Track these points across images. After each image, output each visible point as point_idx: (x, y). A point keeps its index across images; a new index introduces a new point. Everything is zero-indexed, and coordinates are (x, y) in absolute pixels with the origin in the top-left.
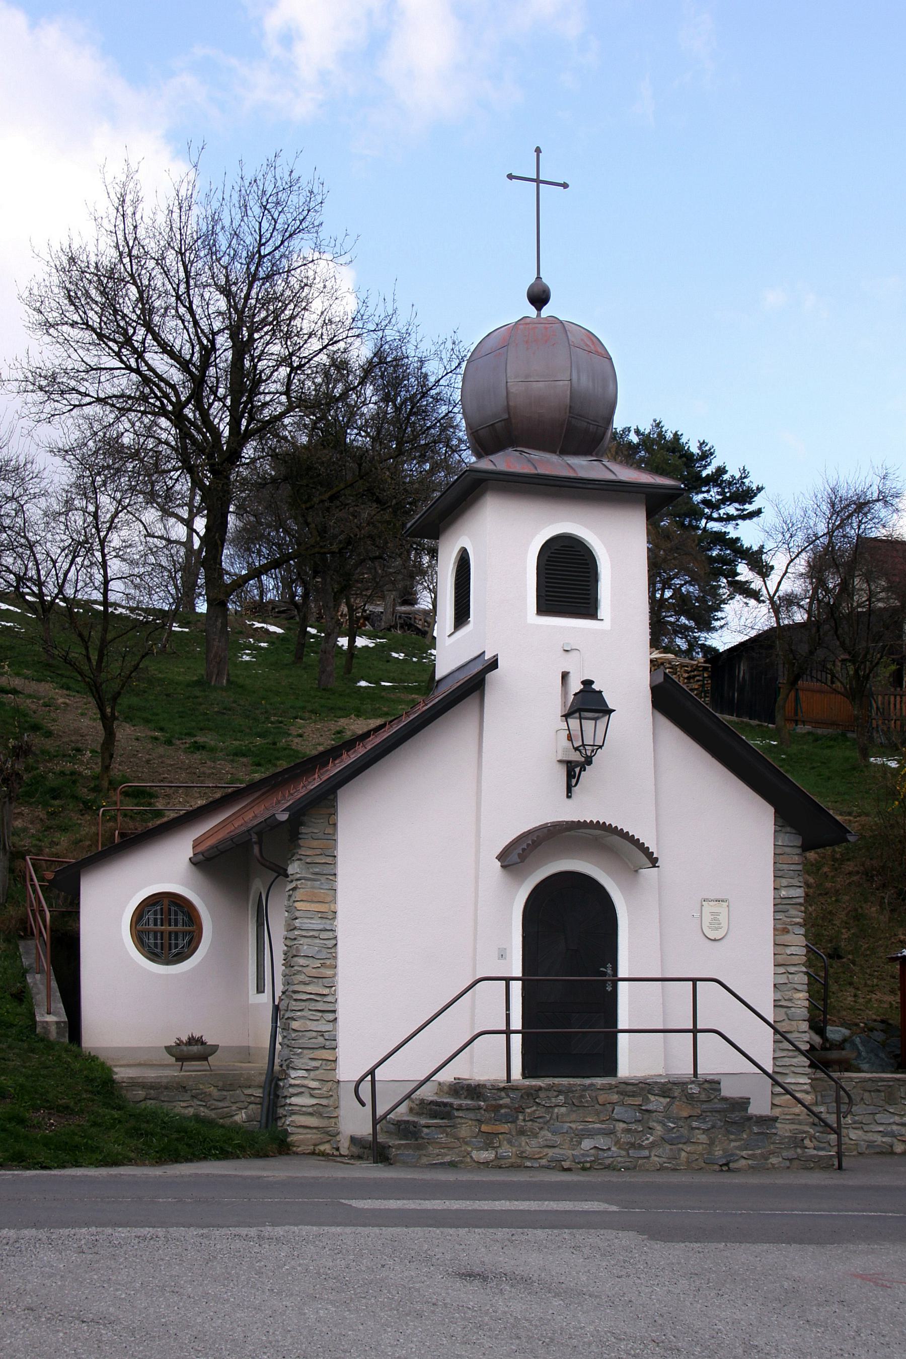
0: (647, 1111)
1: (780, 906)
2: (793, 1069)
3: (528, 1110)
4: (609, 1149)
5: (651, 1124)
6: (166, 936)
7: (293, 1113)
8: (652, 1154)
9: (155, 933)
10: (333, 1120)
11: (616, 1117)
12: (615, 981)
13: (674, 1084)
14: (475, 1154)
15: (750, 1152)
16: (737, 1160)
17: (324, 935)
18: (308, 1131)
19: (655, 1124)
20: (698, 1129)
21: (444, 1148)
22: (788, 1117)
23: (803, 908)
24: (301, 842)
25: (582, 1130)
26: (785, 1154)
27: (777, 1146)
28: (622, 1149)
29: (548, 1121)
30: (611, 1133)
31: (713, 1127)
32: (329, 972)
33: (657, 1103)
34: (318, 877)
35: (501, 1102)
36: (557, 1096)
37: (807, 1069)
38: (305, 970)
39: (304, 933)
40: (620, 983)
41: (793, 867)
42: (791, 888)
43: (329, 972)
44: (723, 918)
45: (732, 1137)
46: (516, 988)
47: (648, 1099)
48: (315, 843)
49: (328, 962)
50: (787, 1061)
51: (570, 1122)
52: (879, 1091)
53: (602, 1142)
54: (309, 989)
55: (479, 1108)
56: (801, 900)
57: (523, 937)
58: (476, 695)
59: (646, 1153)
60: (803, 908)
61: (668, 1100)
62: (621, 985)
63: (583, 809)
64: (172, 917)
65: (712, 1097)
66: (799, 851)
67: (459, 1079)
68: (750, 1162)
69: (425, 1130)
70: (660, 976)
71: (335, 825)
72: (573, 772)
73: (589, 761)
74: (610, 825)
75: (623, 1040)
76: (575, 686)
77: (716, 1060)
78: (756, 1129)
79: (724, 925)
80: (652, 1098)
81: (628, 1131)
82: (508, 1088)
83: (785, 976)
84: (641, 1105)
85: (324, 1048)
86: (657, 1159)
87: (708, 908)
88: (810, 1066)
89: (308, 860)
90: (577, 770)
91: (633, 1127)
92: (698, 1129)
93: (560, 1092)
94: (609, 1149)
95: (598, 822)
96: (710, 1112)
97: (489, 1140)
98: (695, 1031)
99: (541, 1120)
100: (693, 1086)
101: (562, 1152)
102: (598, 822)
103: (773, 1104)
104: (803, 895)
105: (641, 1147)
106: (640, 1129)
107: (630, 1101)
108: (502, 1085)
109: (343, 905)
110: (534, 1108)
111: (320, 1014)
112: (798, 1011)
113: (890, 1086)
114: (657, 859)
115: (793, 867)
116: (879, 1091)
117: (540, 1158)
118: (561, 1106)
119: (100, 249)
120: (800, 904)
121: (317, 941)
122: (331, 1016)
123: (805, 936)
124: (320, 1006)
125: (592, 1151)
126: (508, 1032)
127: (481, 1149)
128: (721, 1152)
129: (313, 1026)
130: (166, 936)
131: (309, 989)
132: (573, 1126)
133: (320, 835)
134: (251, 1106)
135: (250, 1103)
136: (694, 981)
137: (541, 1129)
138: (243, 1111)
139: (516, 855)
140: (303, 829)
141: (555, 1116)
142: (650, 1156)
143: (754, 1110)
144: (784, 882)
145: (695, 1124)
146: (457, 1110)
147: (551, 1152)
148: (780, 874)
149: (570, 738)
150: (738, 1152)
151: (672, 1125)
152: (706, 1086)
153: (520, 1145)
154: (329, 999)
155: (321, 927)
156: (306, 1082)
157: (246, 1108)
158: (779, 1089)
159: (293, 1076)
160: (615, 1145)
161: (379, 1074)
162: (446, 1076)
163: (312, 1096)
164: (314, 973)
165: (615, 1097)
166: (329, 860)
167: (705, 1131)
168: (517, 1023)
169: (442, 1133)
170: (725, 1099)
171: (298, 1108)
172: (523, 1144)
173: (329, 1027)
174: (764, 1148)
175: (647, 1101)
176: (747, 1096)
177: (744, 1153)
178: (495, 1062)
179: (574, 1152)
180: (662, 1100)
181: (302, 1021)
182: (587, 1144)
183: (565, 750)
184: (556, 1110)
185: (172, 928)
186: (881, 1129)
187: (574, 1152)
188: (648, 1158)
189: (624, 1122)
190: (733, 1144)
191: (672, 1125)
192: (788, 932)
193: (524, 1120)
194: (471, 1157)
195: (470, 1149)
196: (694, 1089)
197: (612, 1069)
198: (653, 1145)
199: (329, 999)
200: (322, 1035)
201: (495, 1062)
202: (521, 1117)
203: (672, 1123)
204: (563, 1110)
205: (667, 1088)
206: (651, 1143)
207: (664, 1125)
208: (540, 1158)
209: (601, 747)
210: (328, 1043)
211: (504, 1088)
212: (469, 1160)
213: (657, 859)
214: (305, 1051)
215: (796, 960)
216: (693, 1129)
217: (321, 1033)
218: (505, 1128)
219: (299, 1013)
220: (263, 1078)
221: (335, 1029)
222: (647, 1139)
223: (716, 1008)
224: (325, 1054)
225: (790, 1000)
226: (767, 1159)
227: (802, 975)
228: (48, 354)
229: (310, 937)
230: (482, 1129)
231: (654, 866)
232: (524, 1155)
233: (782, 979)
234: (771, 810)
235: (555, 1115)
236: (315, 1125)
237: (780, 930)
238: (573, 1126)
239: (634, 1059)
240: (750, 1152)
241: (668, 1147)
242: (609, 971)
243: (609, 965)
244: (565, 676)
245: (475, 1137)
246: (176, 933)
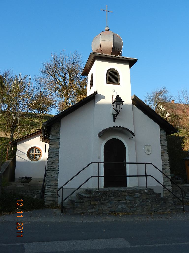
0: (135, 197)
1: (162, 147)
2: (167, 184)
3: (104, 198)
4: (125, 208)
5: (136, 201)
6: (35, 155)
7: (46, 197)
8: (137, 209)
9: (33, 155)
10: (57, 199)
11: (127, 199)
12: (126, 163)
13: (142, 190)
14: (89, 210)
15: (162, 208)
16: (159, 210)
17: (56, 153)
18: (50, 201)
19: (137, 201)
20: (148, 202)
21: (81, 209)
22: (167, 196)
23: (167, 148)
24: (51, 131)
25: (118, 203)
26: (171, 208)
27: (169, 206)
28: (129, 208)
29: (109, 201)
30: (125, 204)
31: (152, 201)
32: (57, 161)
33: (137, 195)
34: (55, 139)
35: (97, 196)
36: (112, 193)
37: (170, 184)
38: (51, 161)
39: (51, 152)
40: (127, 164)
41: (164, 139)
42: (164, 143)
43: (57, 161)
44: (150, 150)
45: (157, 204)
46: (102, 165)
47: (135, 194)
48: (55, 131)
49: (57, 159)
50: (166, 183)
51: (115, 201)
52: (186, 189)
53: (123, 206)
54: (52, 165)
55: (91, 197)
56: (167, 146)
57: (104, 153)
58: (93, 100)
59: (135, 209)
60: (167, 148)
61: (140, 194)
62: (127, 164)
63: (118, 124)
64: (36, 151)
65: (152, 193)
66: (165, 135)
67: (88, 188)
68: (162, 210)
69: (76, 204)
70: (136, 162)
71: (60, 127)
72: (115, 116)
73: (118, 113)
74: (125, 128)
75: (128, 178)
76: (115, 97)
77: (151, 183)
78: (163, 202)
79: (150, 151)
80: (136, 194)
81: (130, 203)
82: (99, 190)
83: (164, 163)
84: (133, 196)
85: (55, 180)
86: (138, 210)
87: (146, 147)
88: (171, 184)
89: (53, 135)
90: (116, 116)
91: (132, 202)
92: (148, 202)
93: (112, 193)
94: (125, 208)
95: (122, 127)
96: (151, 197)
97: (93, 206)
98: (146, 176)
99: (107, 200)
100: (146, 190)
101: (113, 209)
102: (122, 127)
103: (164, 193)
104: (167, 145)
105: (134, 207)
106: (133, 202)
107: (130, 195)
108: (97, 191)
109: (61, 145)
110: (105, 197)
111: (54, 172)
112: (168, 171)
113: (188, 188)
114: (135, 135)
115: (164, 139)
116: (186, 189)
117: (107, 211)
118: (113, 196)
119: (51, 63)
120: (166, 147)
121: (55, 154)
122: (57, 172)
123: (168, 154)
124: (54, 170)
125: (121, 209)
126: (99, 176)
127: (91, 209)
128: (154, 208)
129: (52, 174)
130: (35, 155)
131: (52, 165)
132: (116, 202)
133: (56, 129)
134: (38, 194)
135: (38, 193)
136: (145, 163)
137: (108, 203)
138: (36, 196)
139: (102, 134)
140: (52, 128)
141: (111, 199)
142: (136, 210)
143: (162, 196)
144: (163, 142)
145: (147, 201)
146: (85, 198)
147: (110, 209)
148: (162, 140)
149: (114, 109)
150: (159, 208)
151: (142, 201)
152: (150, 190)
153: (102, 207)
154: (57, 168)
155: (56, 151)
156: (50, 189)
157: (36, 195)
158: (166, 189)
159: (47, 187)
160: (127, 207)
161: (63, 187)
162: (85, 187)
163: (51, 192)
164: (53, 161)
165: (127, 194)
166: (58, 135)
167: (150, 202)
168: (102, 173)
169: (80, 204)
170: (155, 194)
171: (47, 195)
172: (102, 207)
173: (57, 175)
174: (165, 206)
175: (135, 194)
176: (160, 193)
177: (160, 208)
178: (96, 183)
179: (116, 209)
180: (139, 194)
181: (50, 173)
182: (120, 207)
183: (113, 111)
184: (111, 197)
185: (36, 154)
186: (187, 198)
187: (116, 209)
188: (136, 210)
189: (129, 200)
190: (158, 206)
191: (142, 201)
192: (164, 153)
193: (103, 200)
194: (88, 211)
195: (88, 209)
196: (147, 191)
197: (126, 185)
198: (137, 207)
199: (57, 168)
200: (55, 177)
201: (96, 183)
202: (102, 200)
203: (142, 200)
204: (113, 197)
205: (140, 191)
206: (136, 206)
207: (140, 201)
208: (107, 211)
209: (121, 110)
210: (56, 179)
211: (97, 192)
212: (87, 212)
213: (135, 135)
214: (50, 181)
215: (166, 159)
216: (147, 202)
217: (54, 176)
218: (97, 202)
219: (49, 171)
220: (41, 187)
221: (58, 175)
222: (135, 205)
223: (151, 170)
224: (55, 182)
225: (166, 168)
226: (166, 209)
227: (168, 162)
228: (43, 76)
229: (53, 153)
230: (91, 203)
231: (134, 137)
232: (103, 210)
233: (164, 163)
234: (159, 126)
235: (111, 199)
236: (52, 200)
237: (163, 152)
238: (116, 202)
239: (131, 183)
240: (162, 208)
241: (141, 207)
242: (124, 162)
243: (124, 160)
244: (113, 97)
245: (89, 205)
246: (37, 155)
